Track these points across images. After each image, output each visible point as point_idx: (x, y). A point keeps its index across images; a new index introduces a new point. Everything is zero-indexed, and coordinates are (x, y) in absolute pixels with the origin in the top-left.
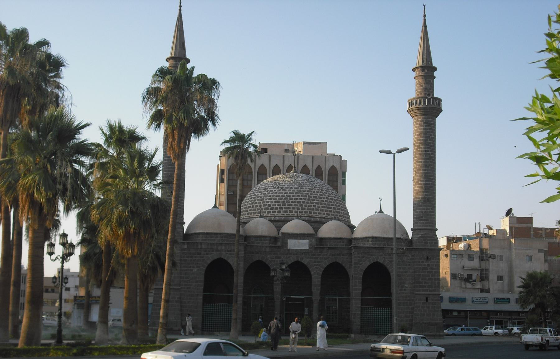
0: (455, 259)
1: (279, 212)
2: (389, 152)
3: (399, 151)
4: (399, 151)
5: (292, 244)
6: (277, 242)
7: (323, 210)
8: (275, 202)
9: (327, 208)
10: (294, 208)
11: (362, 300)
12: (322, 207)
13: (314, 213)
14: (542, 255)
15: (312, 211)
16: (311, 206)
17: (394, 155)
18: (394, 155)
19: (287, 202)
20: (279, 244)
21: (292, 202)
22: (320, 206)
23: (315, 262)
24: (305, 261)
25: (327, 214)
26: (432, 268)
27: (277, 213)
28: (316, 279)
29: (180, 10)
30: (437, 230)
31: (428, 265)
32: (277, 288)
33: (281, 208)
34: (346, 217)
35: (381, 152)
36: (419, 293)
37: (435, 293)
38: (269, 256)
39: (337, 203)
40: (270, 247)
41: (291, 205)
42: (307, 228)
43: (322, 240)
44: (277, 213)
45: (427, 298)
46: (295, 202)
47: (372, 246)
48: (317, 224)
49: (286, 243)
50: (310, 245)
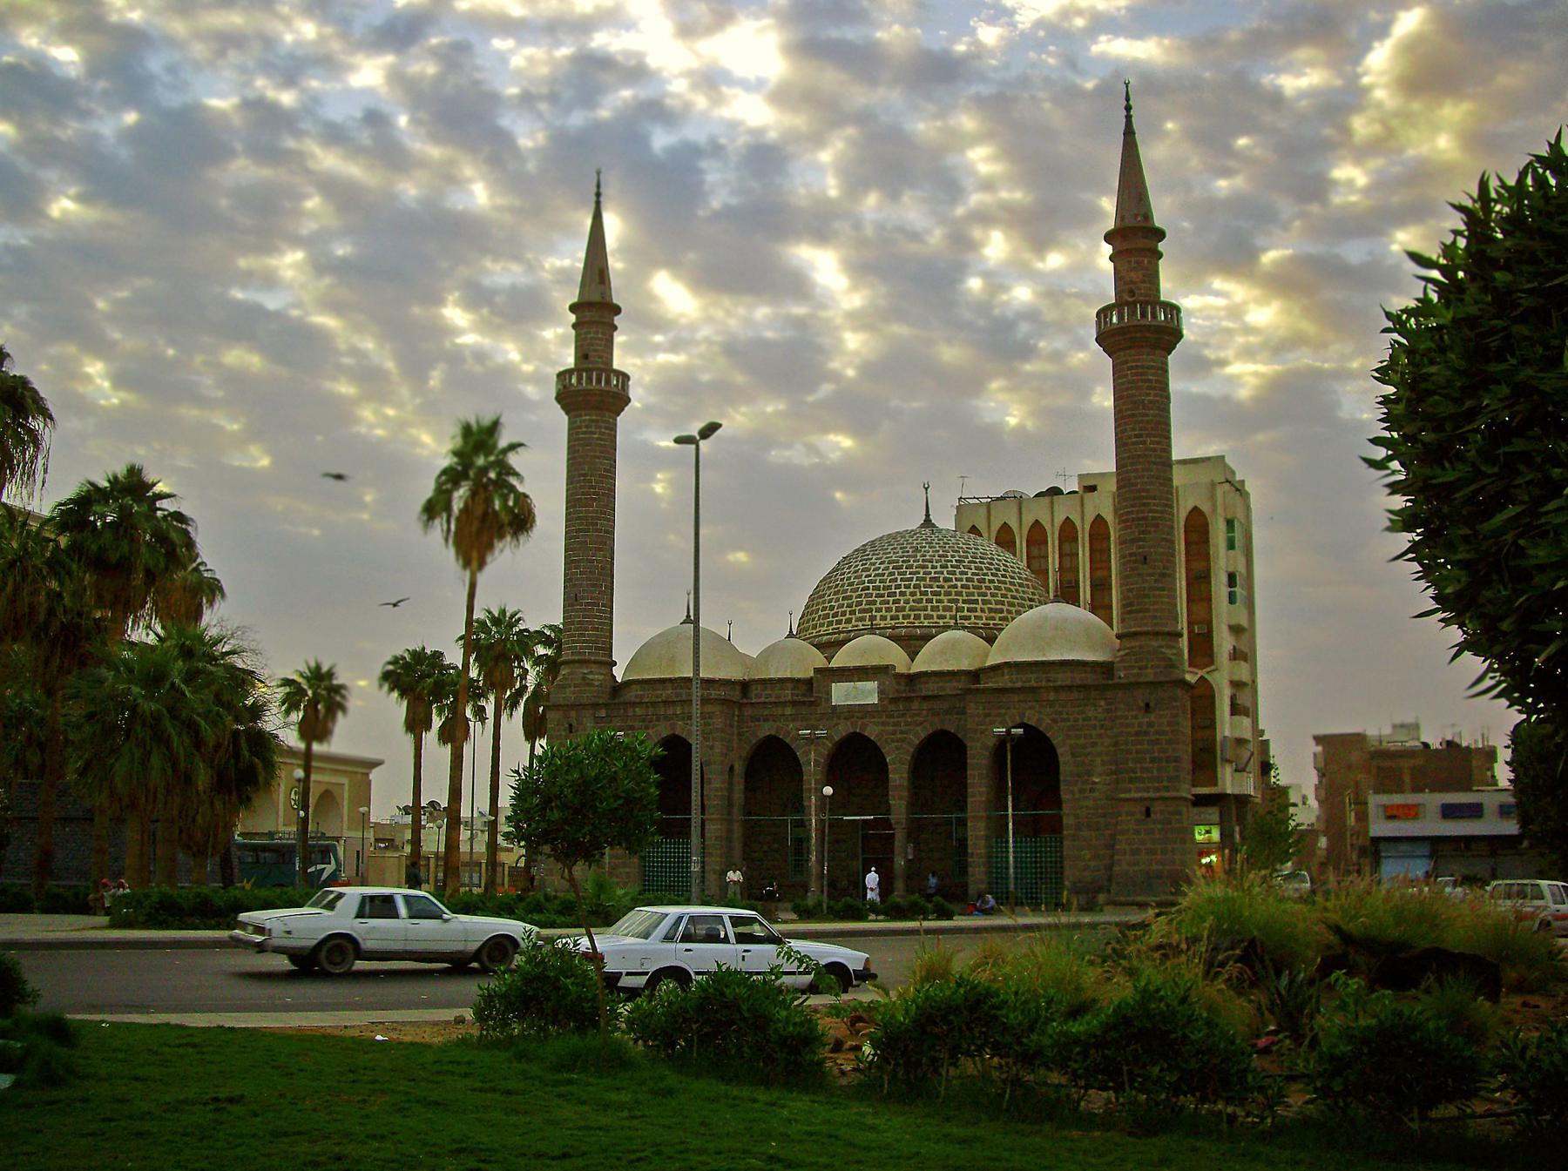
1: (849, 621)
5: (841, 694)
13: (927, 617)
23: (894, 733)
24: (872, 732)
26: (1157, 733)
28: (898, 775)
29: (1128, 118)
31: (1150, 725)
37: (1166, 794)
40: (794, 703)
41: (874, 603)
48: (912, 642)
49: (829, 693)
50: (881, 692)
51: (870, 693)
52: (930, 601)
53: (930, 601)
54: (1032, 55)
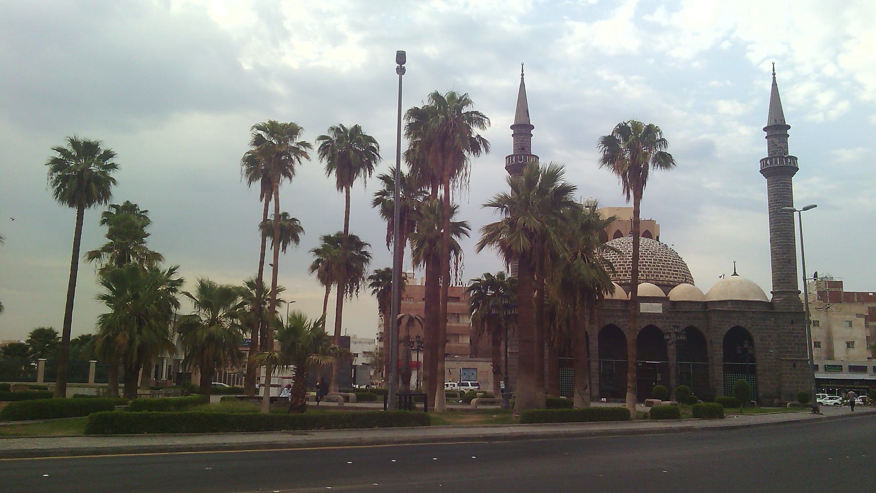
5: (644, 307)
11: (724, 366)
14: (863, 320)
24: (660, 325)
32: (632, 351)
42: (659, 292)
43: (675, 303)
48: (667, 287)
50: (663, 308)
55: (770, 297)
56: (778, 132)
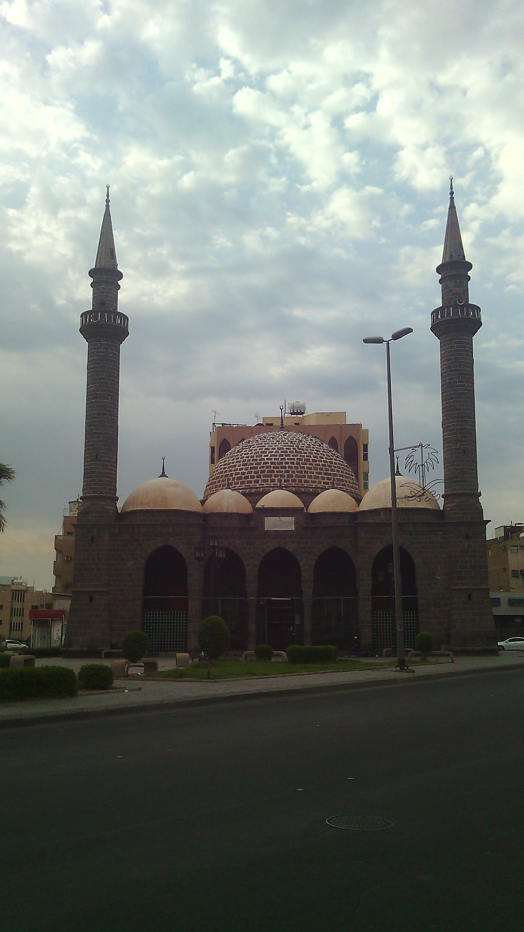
0: (516, 551)
1: (257, 482)
2: (379, 341)
3: (397, 336)
4: (397, 336)
5: (271, 523)
6: (250, 522)
7: (318, 478)
8: (251, 468)
9: (325, 474)
10: (276, 476)
12: (317, 473)
13: (306, 481)
15: (303, 479)
16: (301, 472)
17: (388, 344)
18: (388, 344)
19: (267, 467)
20: (252, 524)
21: (274, 467)
22: (315, 471)
24: (291, 547)
25: (324, 483)
27: (253, 484)
28: (307, 573)
30: (480, 494)
33: (259, 477)
34: (356, 489)
35: (366, 341)
36: (458, 587)
38: (238, 542)
39: (339, 467)
42: (296, 502)
44: (253, 484)
45: (469, 596)
46: (278, 468)
47: (385, 521)
48: (308, 496)
49: (263, 523)
50: (296, 523)
51: (289, 524)
52: (307, 472)
53: (307, 472)
54: (222, 241)
55: (441, 503)
56: (453, 272)
